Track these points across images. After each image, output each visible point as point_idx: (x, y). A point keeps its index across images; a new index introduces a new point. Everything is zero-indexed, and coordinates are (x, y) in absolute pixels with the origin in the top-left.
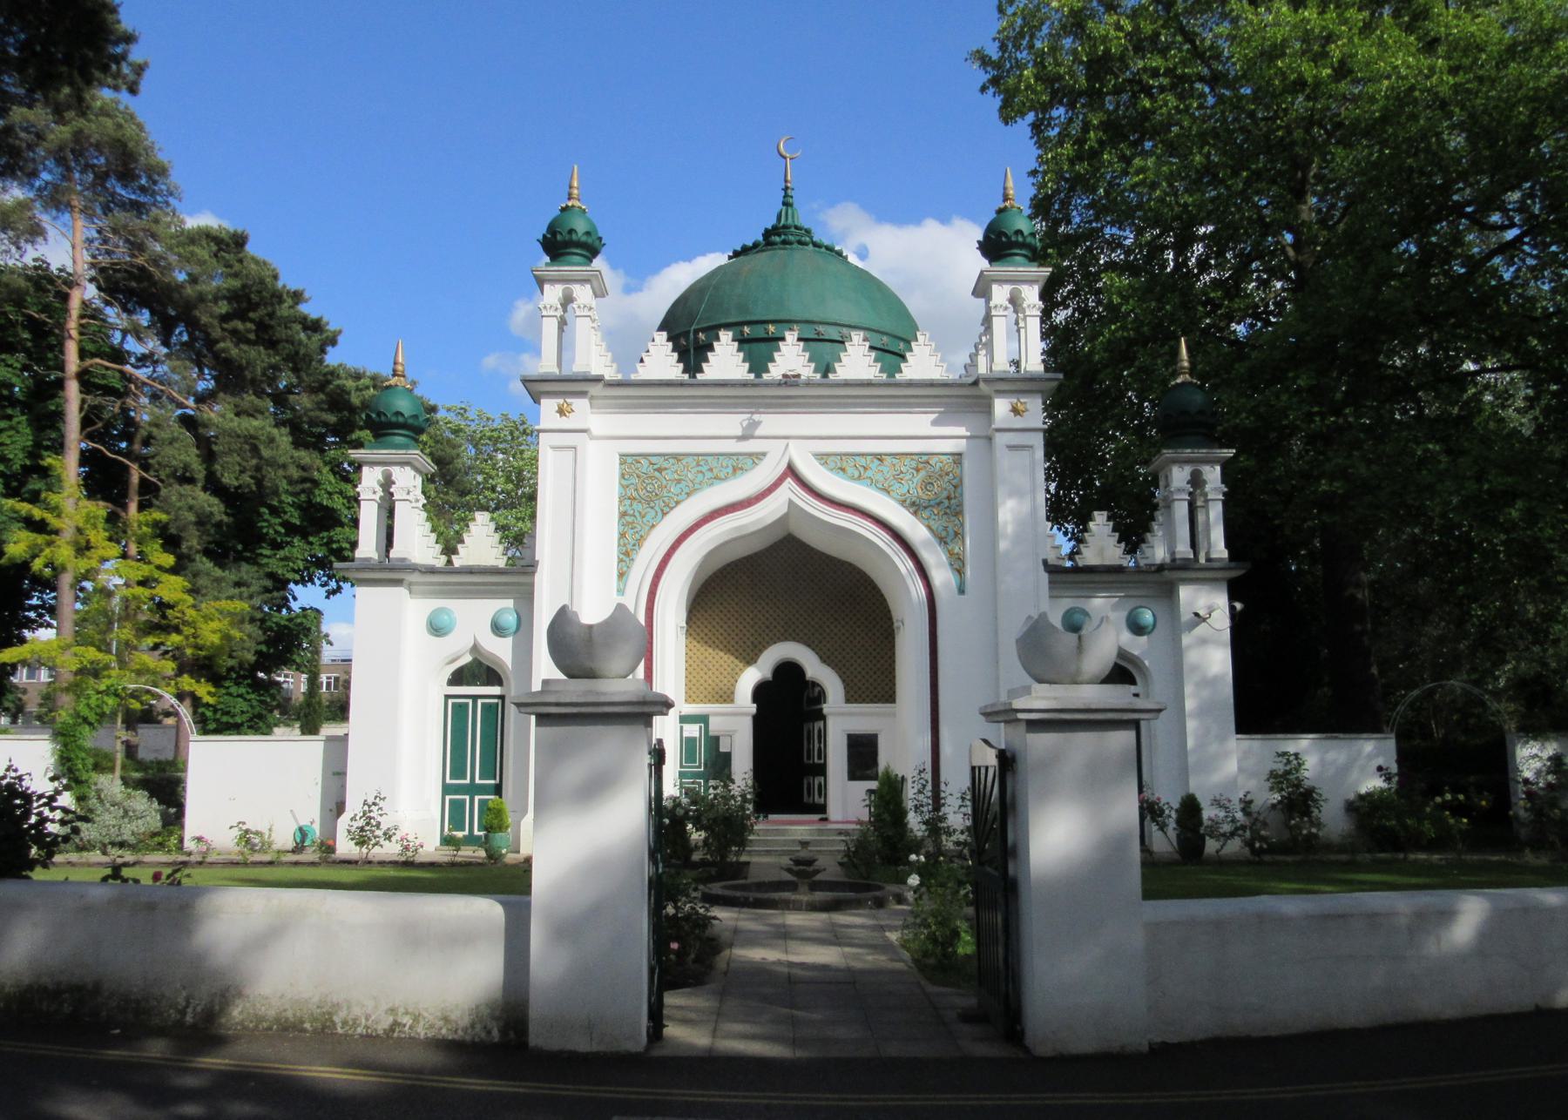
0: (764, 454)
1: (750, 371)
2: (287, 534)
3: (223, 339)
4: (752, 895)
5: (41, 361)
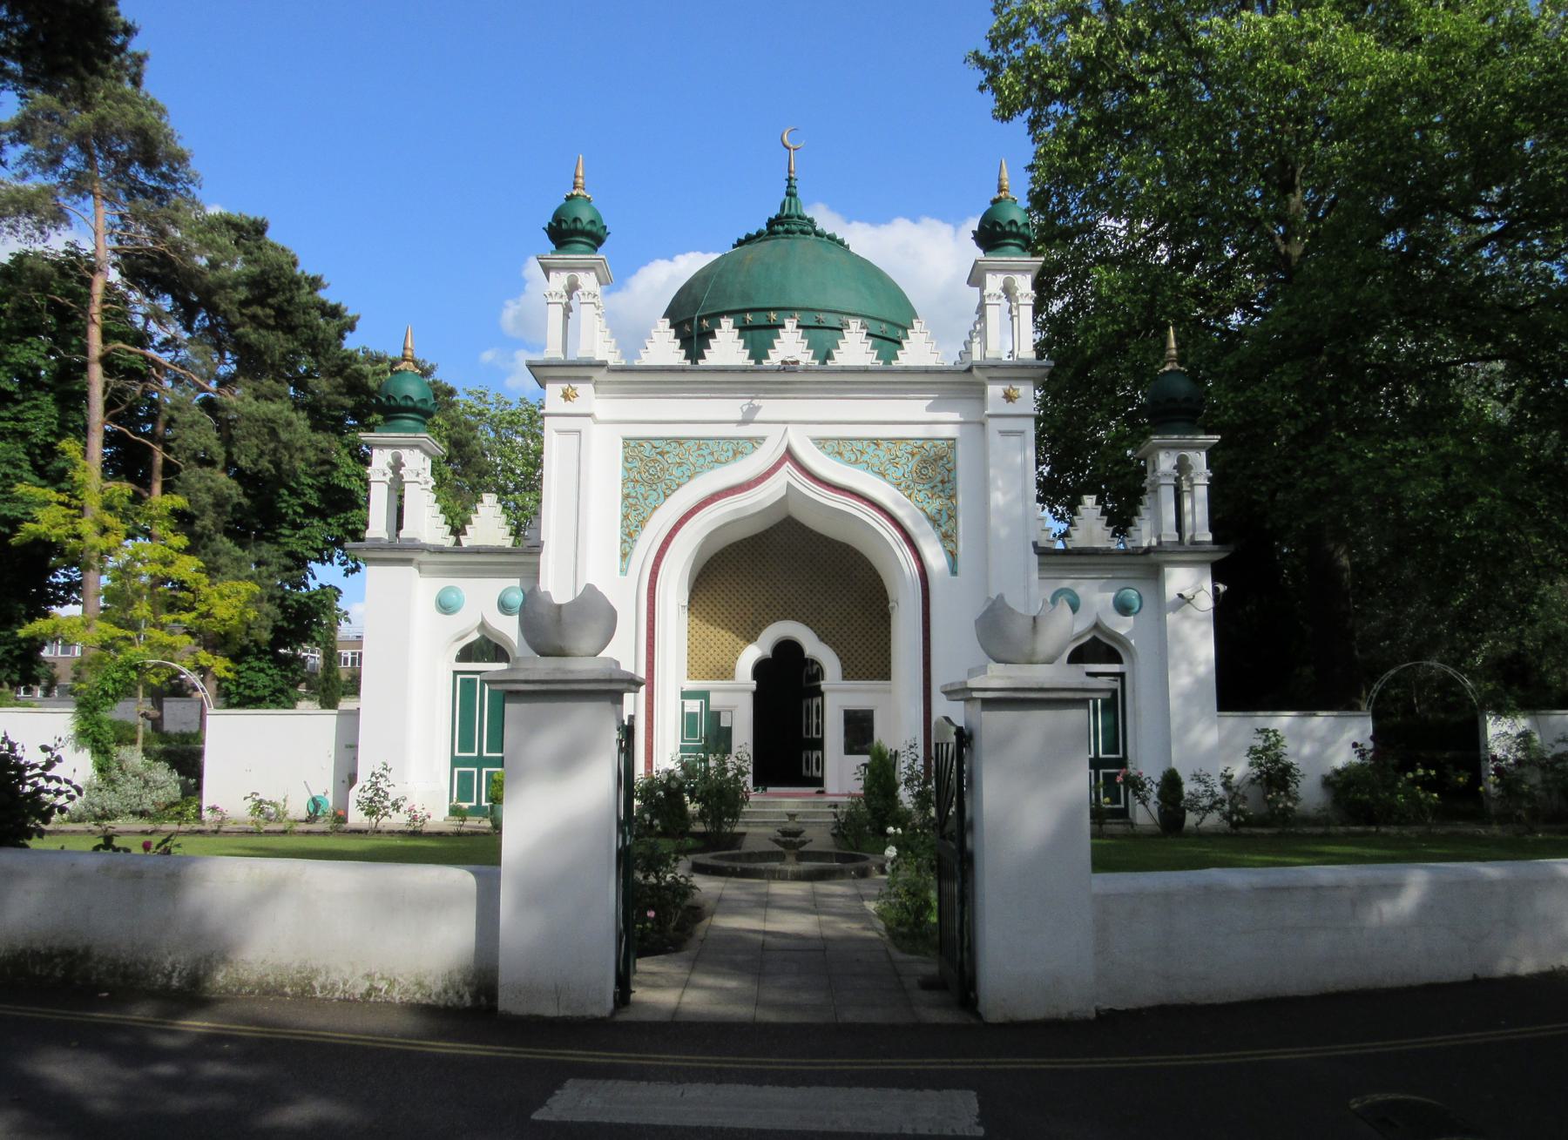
0: (763, 439)
1: (750, 357)
2: (306, 516)
3: (243, 324)
4: (739, 865)
5: (66, 346)
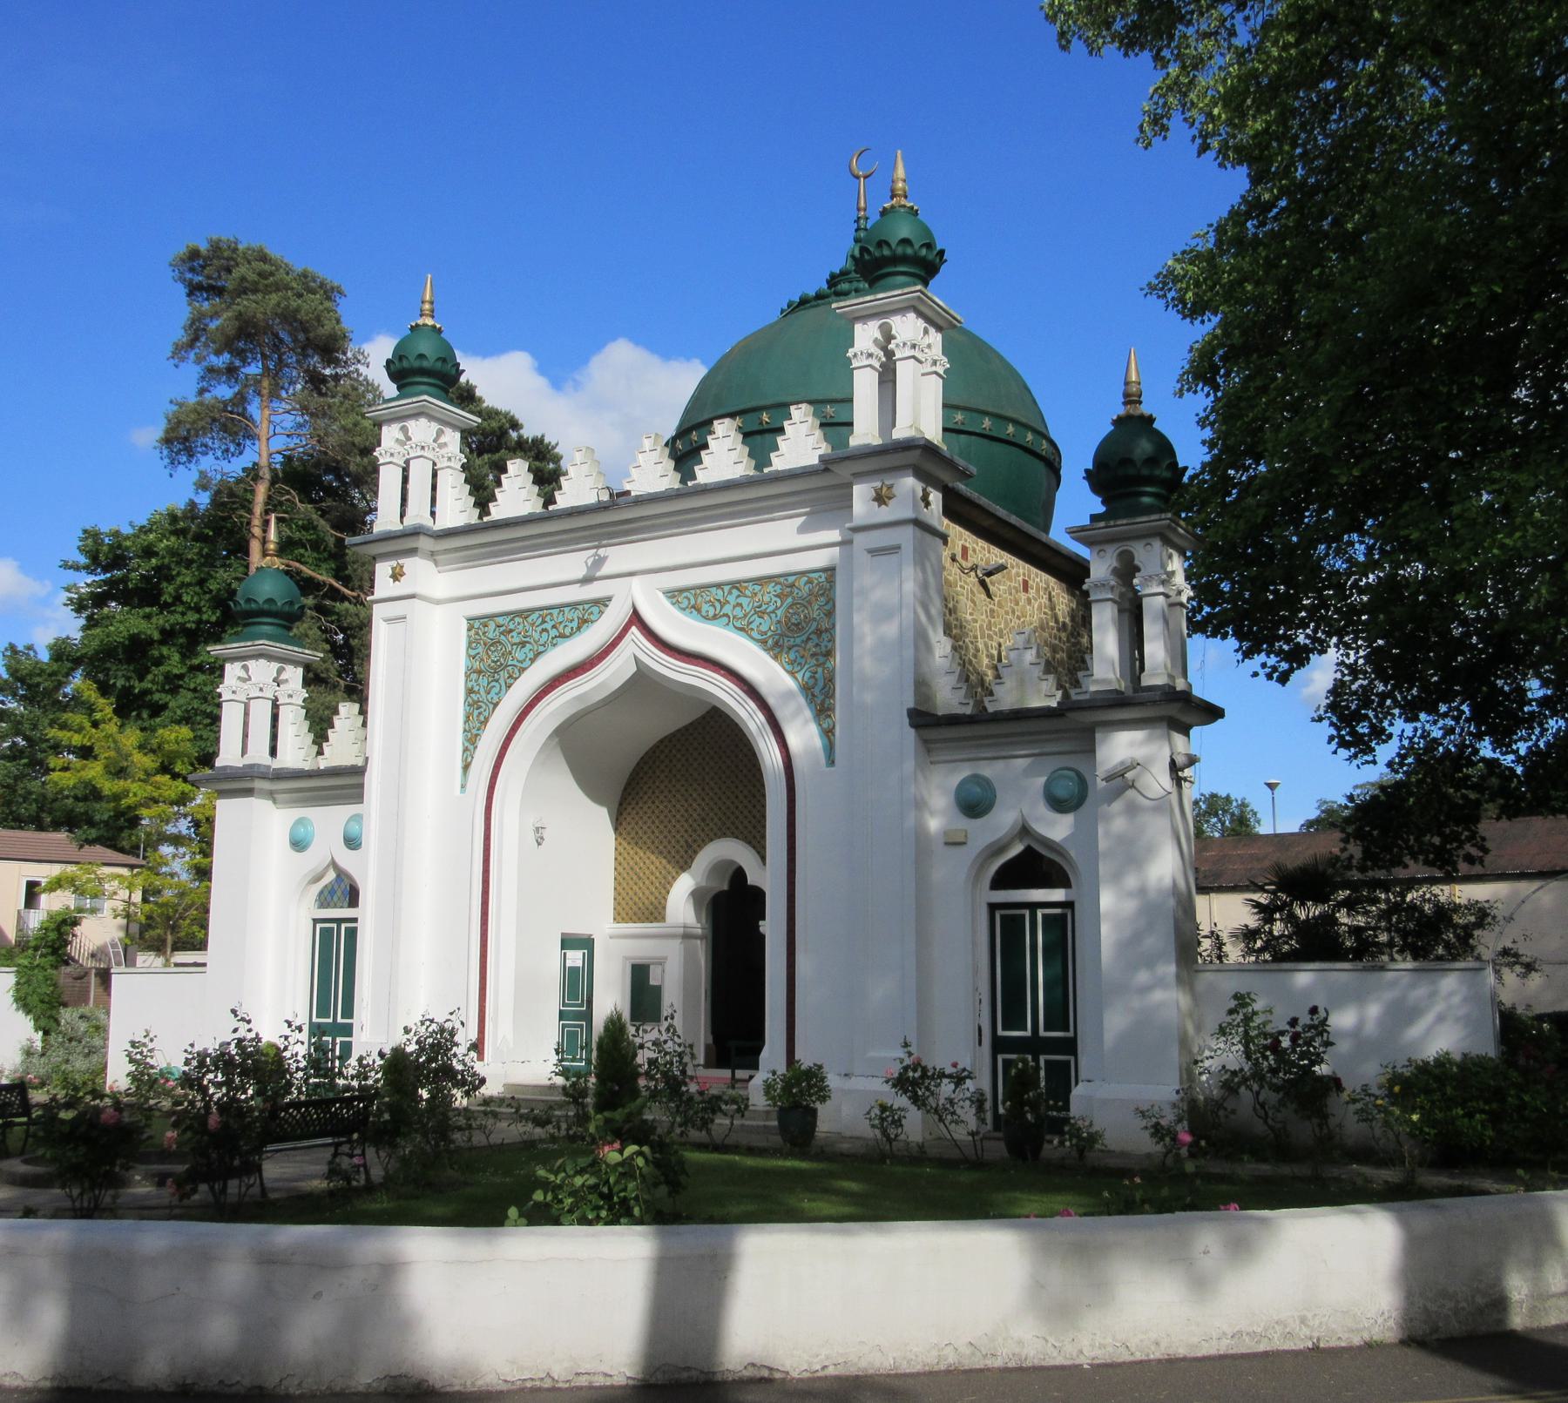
0: (609, 599)
